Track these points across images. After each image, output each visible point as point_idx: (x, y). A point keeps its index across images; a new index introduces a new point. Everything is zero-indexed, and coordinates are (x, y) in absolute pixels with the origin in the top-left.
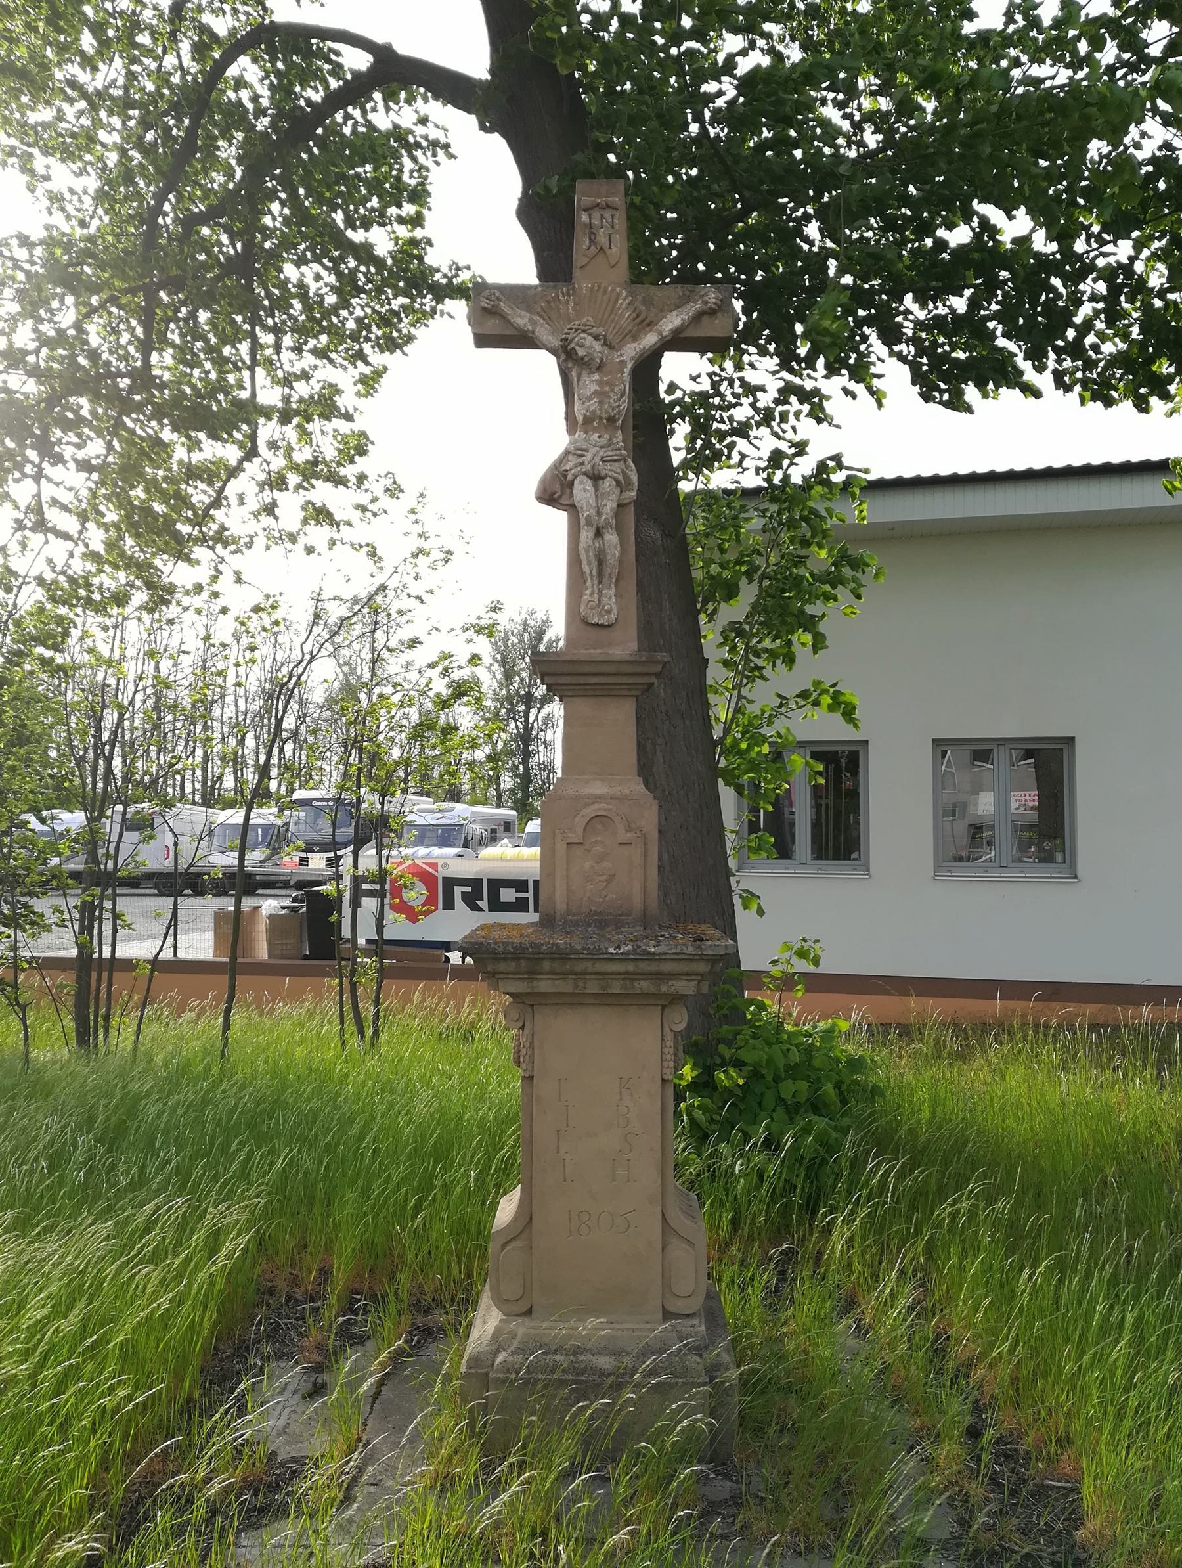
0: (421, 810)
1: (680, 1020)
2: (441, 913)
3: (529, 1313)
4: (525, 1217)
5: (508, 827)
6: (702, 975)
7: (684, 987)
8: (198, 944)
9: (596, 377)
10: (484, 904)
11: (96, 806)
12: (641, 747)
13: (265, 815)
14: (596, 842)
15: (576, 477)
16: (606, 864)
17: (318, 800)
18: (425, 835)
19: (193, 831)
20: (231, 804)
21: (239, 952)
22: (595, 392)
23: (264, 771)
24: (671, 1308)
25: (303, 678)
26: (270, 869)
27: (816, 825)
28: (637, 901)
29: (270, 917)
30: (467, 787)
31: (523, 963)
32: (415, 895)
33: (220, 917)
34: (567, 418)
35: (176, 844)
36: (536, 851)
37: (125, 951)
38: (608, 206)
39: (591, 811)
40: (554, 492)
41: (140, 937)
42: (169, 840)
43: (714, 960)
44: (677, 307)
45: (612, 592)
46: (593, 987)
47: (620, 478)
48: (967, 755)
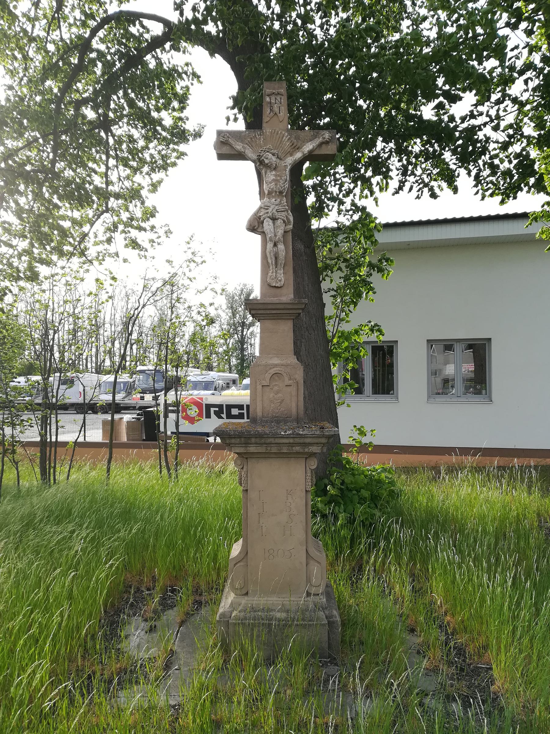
0: (194, 374)
1: (314, 464)
2: (204, 420)
3: (247, 594)
4: (245, 553)
5: (234, 382)
7: (315, 449)
8: (95, 435)
9: (274, 173)
10: (224, 416)
11: (46, 373)
12: (295, 343)
13: (124, 377)
14: (276, 385)
16: (280, 395)
17: (148, 370)
18: (196, 385)
19: (91, 384)
20: (109, 373)
21: (114, 438)
23: (123, 357)
25: (140, 315)
26: (127, 401)
27: (374, 380)
28: (294, 411)
29: (128, 422)
30: (216, 364)
31: (243, 439)
32: (193, 412)
33: (105, 423)
34: (260, 194)
35: (84, 390)
36: (248, 392)
37: (62, 438)
39: (272, 371)
40: (255, 226)
41: (69, 432)
42: (81, 389)
43: (329, 437)
44: (311, 140)
46: (274, 450)
47: (285, 219)
48: (442, 348)
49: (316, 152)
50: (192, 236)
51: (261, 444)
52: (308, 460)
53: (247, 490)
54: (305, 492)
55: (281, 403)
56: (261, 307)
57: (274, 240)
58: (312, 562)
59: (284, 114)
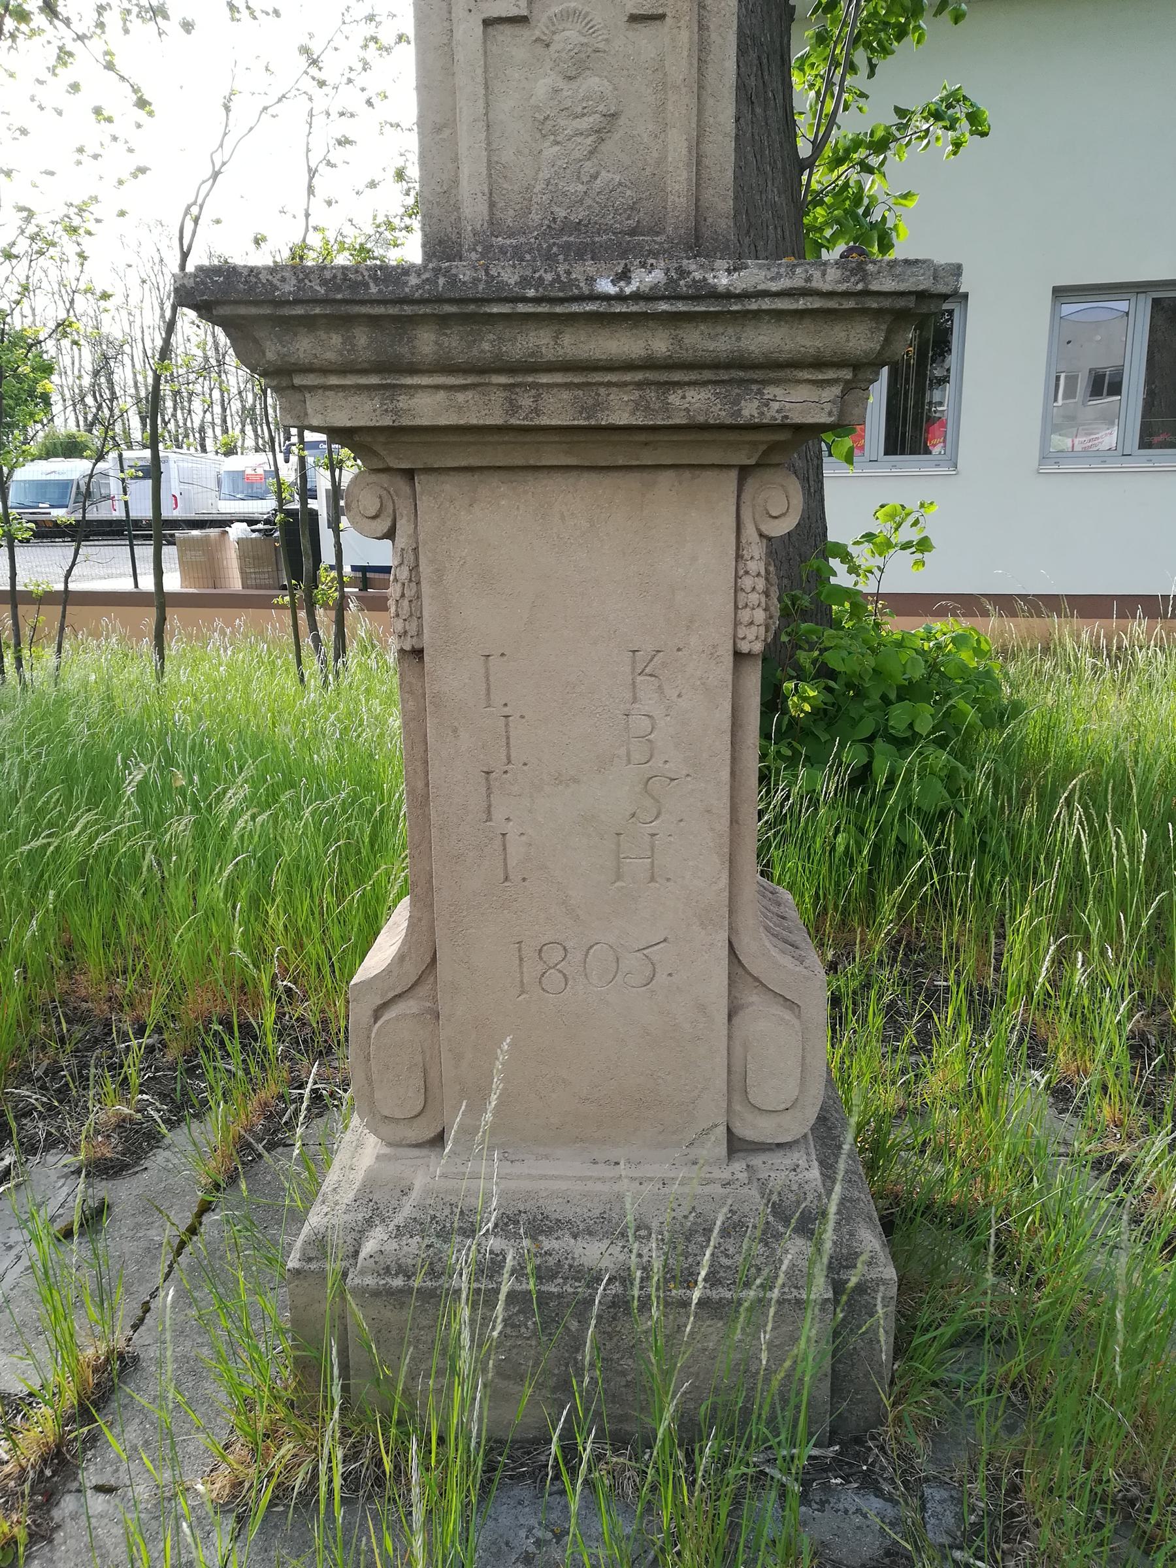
4: (423, 965)
6: (856, 366)
16: (593, 83)
24: (745, 1132)
29: (240, 541)
51: (480, 369)
52: (751, 485)
53: (418, 653)
54: (729, 659)
55: (601, 133)
58: (753, 998)
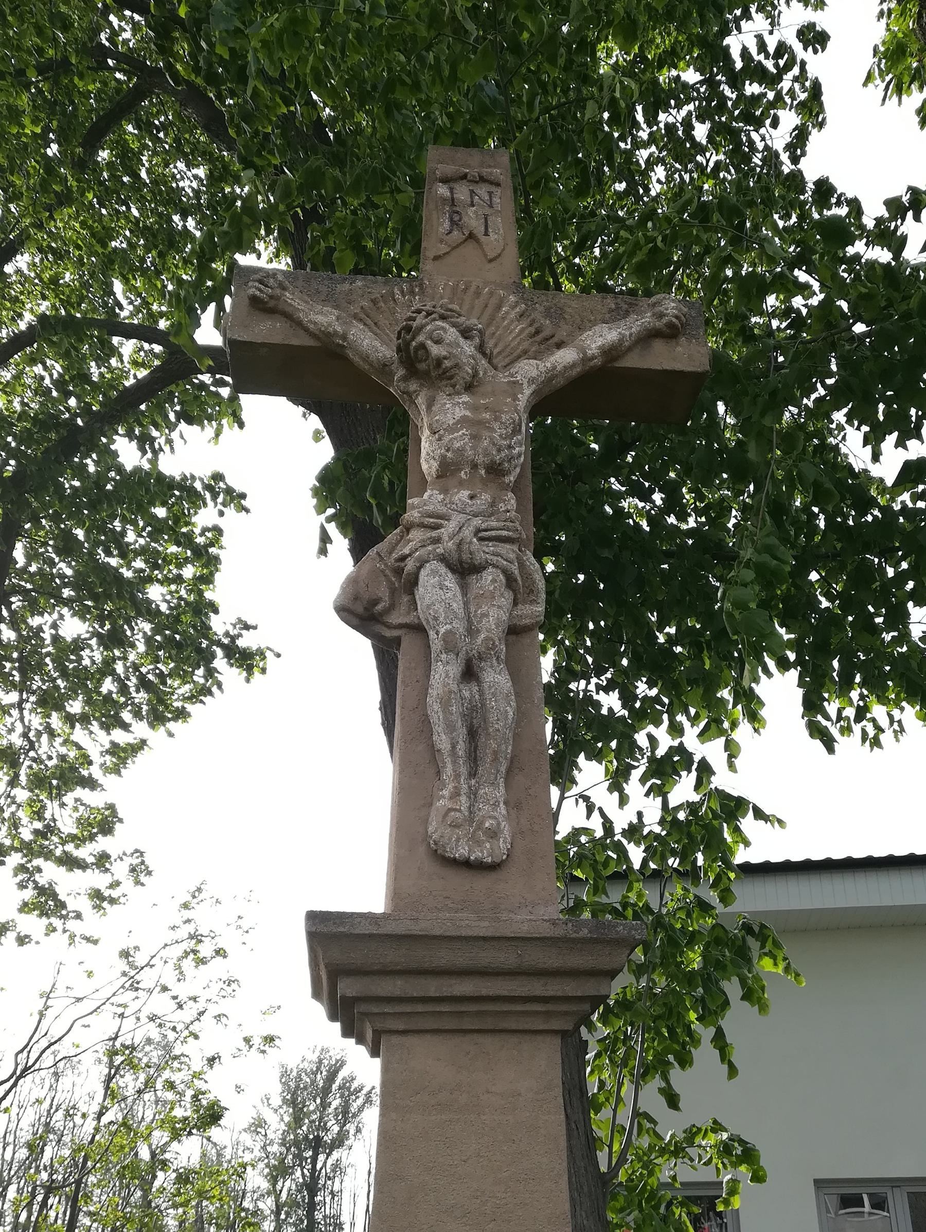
9: (465, 398)
15: (422, 564)
22: (463, 421)
38: (482, 180)
45: (500, 792)
47: (515, 569)
49: (632, 361)
50: (199, 890)
56: (393, 956)
57: (464, 645)
59: (502, 235)
